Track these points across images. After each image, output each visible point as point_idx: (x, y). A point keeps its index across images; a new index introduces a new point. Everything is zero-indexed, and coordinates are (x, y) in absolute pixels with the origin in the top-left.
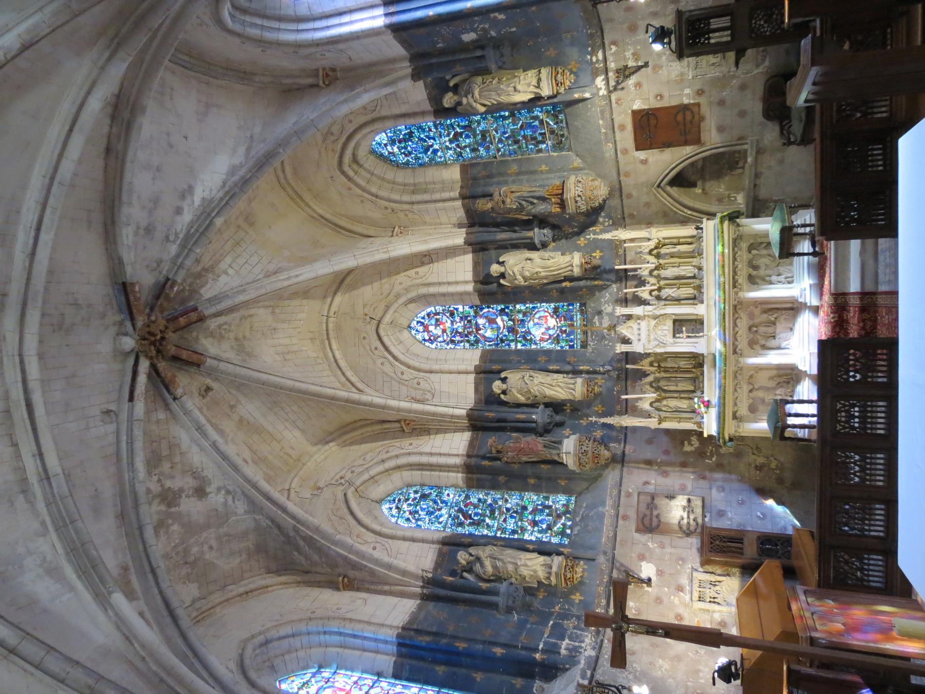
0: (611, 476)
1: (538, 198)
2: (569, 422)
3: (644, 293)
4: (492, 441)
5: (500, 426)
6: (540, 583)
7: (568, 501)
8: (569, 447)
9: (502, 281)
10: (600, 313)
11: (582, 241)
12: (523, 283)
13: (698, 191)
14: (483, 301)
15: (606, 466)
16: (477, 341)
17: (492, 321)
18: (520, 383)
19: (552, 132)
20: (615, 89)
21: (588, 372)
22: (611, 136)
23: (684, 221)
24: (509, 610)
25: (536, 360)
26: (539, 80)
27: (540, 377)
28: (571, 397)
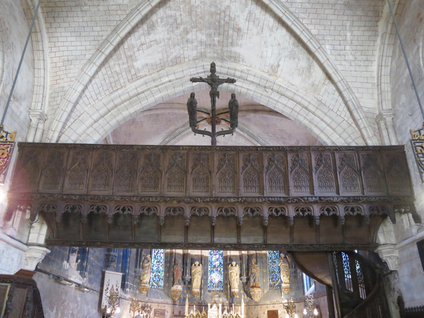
0: (170, 301)
1: (255, 279)
2: (185, 286)
3: (225, 312)
4: (180, 261)
5: (184, 264)
6: (141, 281)
7: (161, 287)
8: (179, 287)
9: (230, 265)
10: (220, 297)
11: (242, 292)
12: (229, 272)
14: (224, 257)
15: (173, 299)
16: (211, 254)
17: (217, 260)
18: (198, 271)
19: (275, 284)
20: (284, 305)
21: (201, 293)
22: (272, 303)
24: (135, 272)
25: (205, 275)
26: (286, 283)
27: (200, 277)
28: (193, 287)
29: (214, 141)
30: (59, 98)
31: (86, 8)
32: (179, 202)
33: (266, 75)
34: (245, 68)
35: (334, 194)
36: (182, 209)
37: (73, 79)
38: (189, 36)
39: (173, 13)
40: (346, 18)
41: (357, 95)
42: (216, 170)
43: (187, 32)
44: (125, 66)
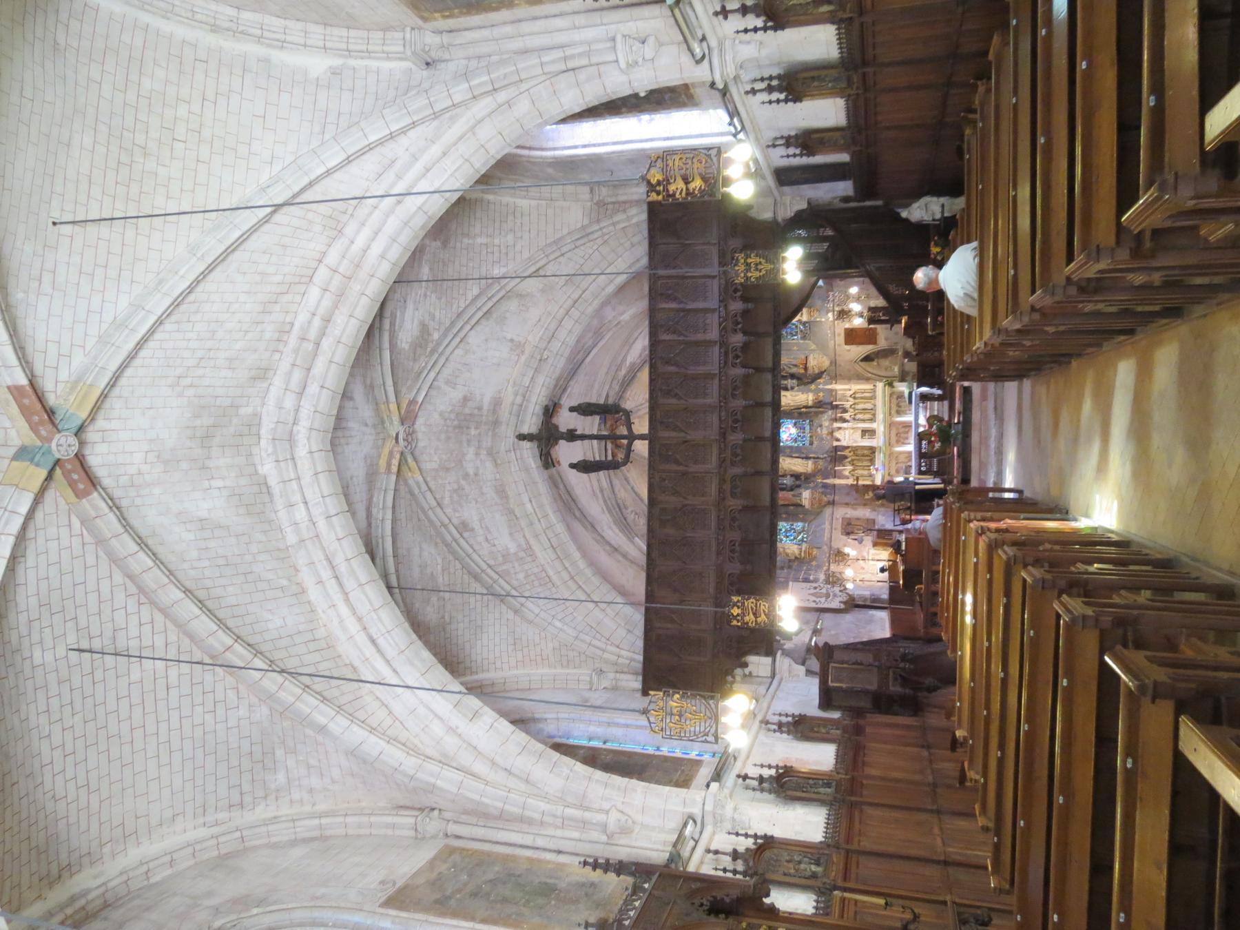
0: (828, 511)
3: (847, 416)
8: (806, 496)
11: (813, 387)
13: (875, 363)
23: (867, 380)
29: (642, 437)
30: (571, 654)
31: (447, 617)
32: (724, 481)
33: (523, 358)
34: (510, 388)
35: (716, 282)
36: (734, 478)
37: (543, 634)
38: (471, 472)
39: (447, 494)
40: (458, 244)
41: (565, 231)
42: (682, 434)
43: (466, 476)
44: (516, 565)
